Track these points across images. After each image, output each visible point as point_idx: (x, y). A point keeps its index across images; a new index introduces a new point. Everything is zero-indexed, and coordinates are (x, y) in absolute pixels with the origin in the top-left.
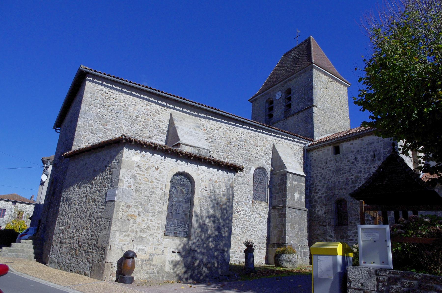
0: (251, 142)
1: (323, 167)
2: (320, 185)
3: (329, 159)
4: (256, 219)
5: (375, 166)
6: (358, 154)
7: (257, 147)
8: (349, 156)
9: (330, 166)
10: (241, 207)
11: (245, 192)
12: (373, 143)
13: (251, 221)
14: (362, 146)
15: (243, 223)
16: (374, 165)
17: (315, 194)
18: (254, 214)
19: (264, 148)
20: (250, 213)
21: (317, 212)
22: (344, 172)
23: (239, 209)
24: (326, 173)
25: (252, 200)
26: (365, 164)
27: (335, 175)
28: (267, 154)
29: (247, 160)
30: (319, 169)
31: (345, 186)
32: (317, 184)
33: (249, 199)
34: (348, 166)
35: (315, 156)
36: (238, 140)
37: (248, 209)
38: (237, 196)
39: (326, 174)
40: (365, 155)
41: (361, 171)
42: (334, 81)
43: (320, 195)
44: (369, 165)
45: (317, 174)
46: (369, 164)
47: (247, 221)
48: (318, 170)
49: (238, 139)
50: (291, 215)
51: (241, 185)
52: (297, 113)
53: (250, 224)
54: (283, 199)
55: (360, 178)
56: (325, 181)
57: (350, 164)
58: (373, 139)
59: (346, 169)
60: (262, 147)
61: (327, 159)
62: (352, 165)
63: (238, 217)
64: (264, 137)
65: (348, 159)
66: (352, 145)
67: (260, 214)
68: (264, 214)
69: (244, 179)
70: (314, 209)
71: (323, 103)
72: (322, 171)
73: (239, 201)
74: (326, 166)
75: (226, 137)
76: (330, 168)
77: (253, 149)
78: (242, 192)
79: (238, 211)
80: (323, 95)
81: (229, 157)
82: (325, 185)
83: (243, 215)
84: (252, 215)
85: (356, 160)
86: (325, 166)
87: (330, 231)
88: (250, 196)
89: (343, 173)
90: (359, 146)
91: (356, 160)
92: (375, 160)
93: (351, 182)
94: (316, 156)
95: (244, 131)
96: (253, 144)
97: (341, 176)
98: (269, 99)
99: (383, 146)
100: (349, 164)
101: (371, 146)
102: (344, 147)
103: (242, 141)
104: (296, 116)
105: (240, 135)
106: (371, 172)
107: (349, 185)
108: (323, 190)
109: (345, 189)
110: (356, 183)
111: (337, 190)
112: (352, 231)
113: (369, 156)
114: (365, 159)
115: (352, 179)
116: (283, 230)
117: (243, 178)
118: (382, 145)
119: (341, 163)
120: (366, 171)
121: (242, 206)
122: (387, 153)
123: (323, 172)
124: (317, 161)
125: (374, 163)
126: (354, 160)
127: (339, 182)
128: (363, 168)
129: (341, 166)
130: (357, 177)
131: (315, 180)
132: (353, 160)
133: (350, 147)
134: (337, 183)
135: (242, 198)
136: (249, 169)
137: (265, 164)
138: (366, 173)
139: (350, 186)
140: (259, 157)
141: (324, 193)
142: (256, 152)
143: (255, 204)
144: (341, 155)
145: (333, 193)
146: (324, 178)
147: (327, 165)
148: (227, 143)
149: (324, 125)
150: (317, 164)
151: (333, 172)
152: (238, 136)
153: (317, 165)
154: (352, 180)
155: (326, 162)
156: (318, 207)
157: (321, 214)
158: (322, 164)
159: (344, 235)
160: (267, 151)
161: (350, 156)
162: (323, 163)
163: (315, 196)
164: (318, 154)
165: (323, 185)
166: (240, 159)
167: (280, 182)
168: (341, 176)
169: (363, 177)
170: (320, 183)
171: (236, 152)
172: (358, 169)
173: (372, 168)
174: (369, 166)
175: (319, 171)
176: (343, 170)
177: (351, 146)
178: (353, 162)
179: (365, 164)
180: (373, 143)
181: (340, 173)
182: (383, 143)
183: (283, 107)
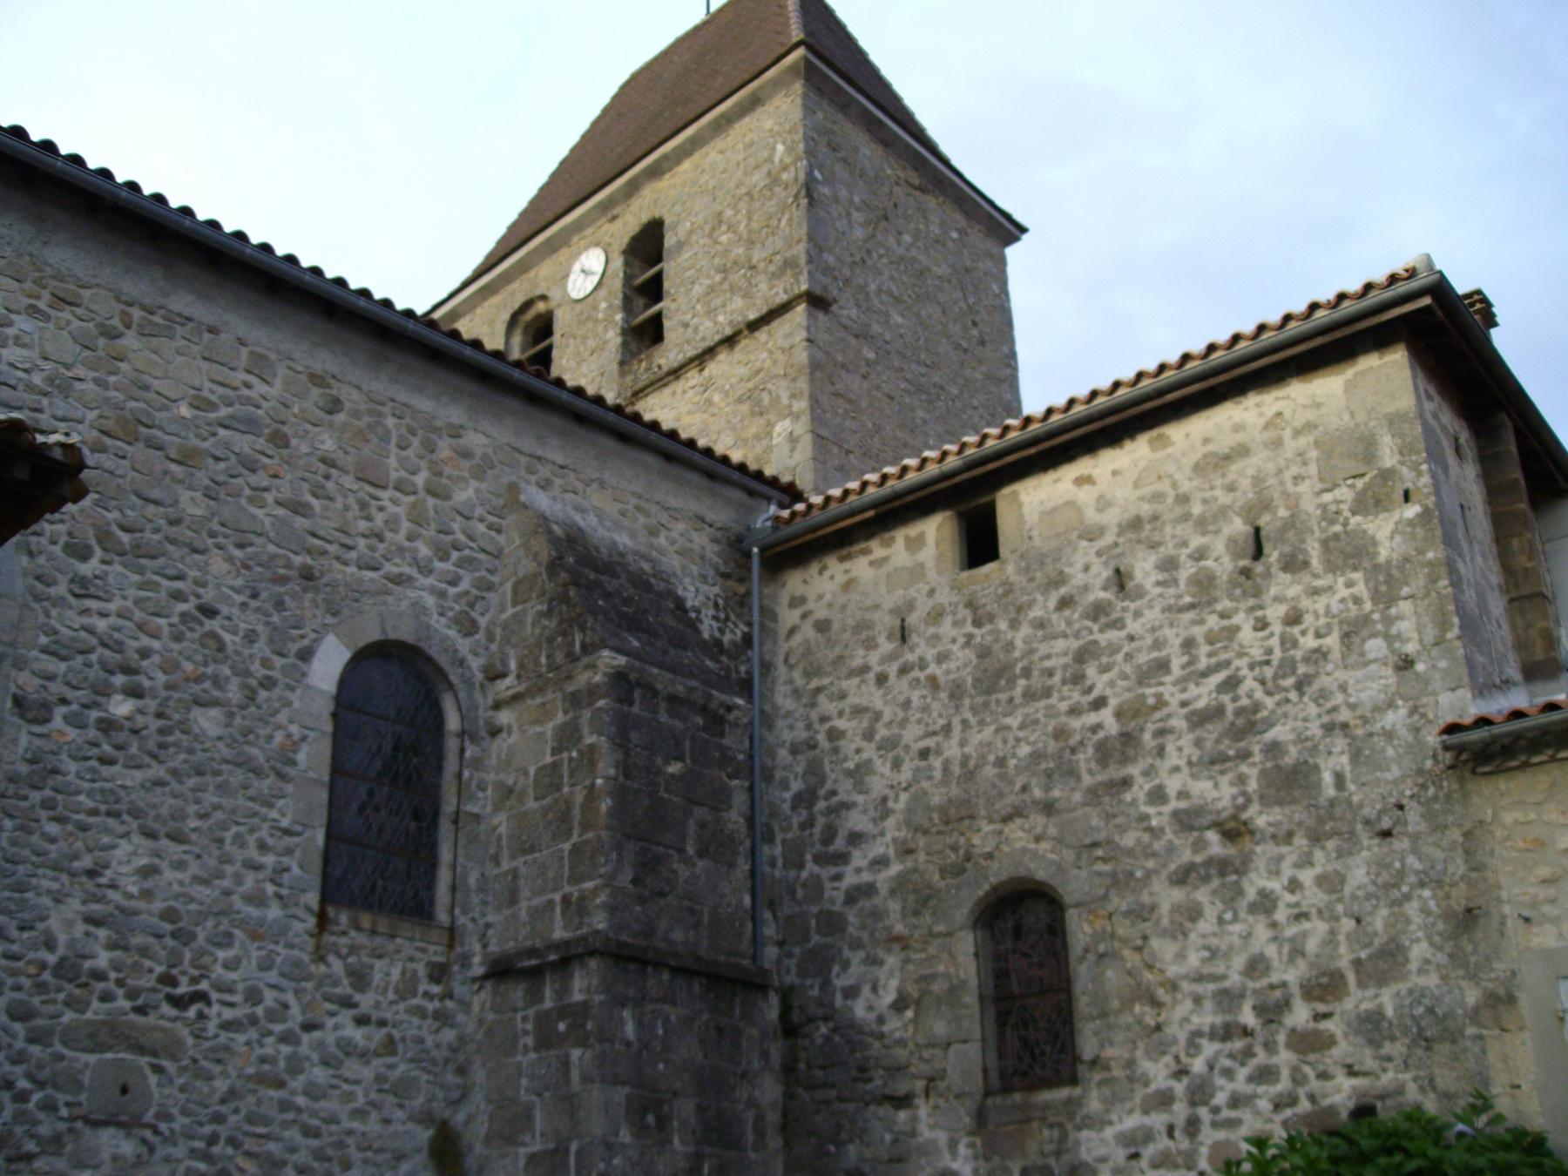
0: (328, 444)
1: (877, 669)
2: (860, 799)
3: (923, 607)
4: (352, 1068)
5: (1270, 619)
6: (1139, 542)
7: (379, 493)
8: (1067, 570)
9: (930, 654)
10: (206, 960)
11: (252, 831)
12: (1242, 451)
13: (297, 1083)
14: (1165, 486)
15: (223, 1101)
16: (1261, 607)
17: (826, 872)
18: (330, 1022)
19: (431, 502)
20: (295, 1010)
21: (839, 1000)
22: (1036, 681)
23: (194, 980)
24: (907, 704)
25: (312, 899)
26: (1192, 606)
27: (969, 716)
28: (455, 555)
29: (284, 580)
30: (855, 681)
31: (1048, 789)
32: (835, 800)
33: (285, 892)
34: (1065, 636)
35: (820, 597)
36: (212, 416)
37: (272, 976)
38: (180, 865)
39: (901, 714)
40: (1185, 544)
41: (1163, 666)
42: (930, 187)
43: (858, 871)
44: (1223, 615)
45: (840, 724)
46: (1219, 607)
47: (261, 1079)
48: (843, 696)
49: (212, 406)
50: (640, 1024)
51: (217, 773)
52: (705, 356)
53: (285, 1106)
54: (567, 889)
55: (1158, 715)
56: (897, 765)
57: (1077, 626)
58: (1238, 428)
59: (1048, 664)
60: (422, 494)
61: (910, 606)
62: (1091, 632)
63: (179, 1042)
64: (438, 423)
65: (1063, 591)
66: (1087, 487)
67: (382, 1023)
68: (416, 1021)
69: (247, 732)
70: (817, 982)
71: (867, 298)
72: (874, 697)
73: (193, 907)
74: (901, 661)
75: (112, 379)
76: (933, 669)
77: (340, 499)
78: (228, 835)
79: (183, 989)
80: (869, 251)
81: (125, 538)
82: (896, 800)
83: (227, 1026)
84: (309, 1027)
85: (1122, 587)
86: (891, 657)
87: (942, 1137)
88: (296, 870)
89: (1029, 696)
90: (1136, 485)
91: (1122, 587)
92: (1268, 575)
93: (1090, 750)
94: (828, 597)
95: (273, 356)
96: (349, 461)
97: (1014, 722)
98: (528, 304)
99: (1313, 469)
100: (1069, 623)
101: (1231, 477)
102: (1026, 509)
103: (250, 426)
104: (693, 378)
105: (238, 383)
106: (1237, 663)
107: (1078, 778)
108: (882, 834)
109: (1048, 808)
110: (1125, 760)
111: (987, 828)
112: (1111, 1123)
113: (1219, 547)
114: (1187, 571)
115: (1095, 728)
116: (567, 1151)
117: (238, 721)
118: (1305, 464)
119: (1014, 624)
120: (1203, 663)
121: (222, 954)
122: (1347, 513)
123: (878, 704)
124: (836, 626)
125: (1256, 595)
126: (1105, 589)
127: (1001, 762)
128: (1178, 641)
129: (1010, 646)
130: (1131, 713)
131: (827, 768)
132: (1102, 595)
133: (1071, 504)
134: (990, 771)
135: (226, 883)
136: (294, 647)
137: (439, 624)
138: (1205, 674)
139: (1087, 780)
140: (390, 568)
141: (891, 852)
142: (363, 525)
143: (343, 941)
144: (1010, 569)
145: (955, 848)
146: (888, 745)
147: (912, 649)
148: (117, 430)
149: (878, 429)
150: (837, 651)
151: (956, 693)
152: (220, 390)
153: (840, 659)
154: (1101, 735)
155: (903, 628)
156: (846, 965)
157: (872, 1017)
158: (870, 644)
159: (1052, 1161)
160: (456, 526)
161: (1079, 566)
162: (882, 640)
163: (828, 885)
164: (841, 579)
165: (885, 800)
166: (218, 565)
167: (549, 759)
168: (1014, 722)
169: (1184, 704)
170: (860, 787)
171: (192, 505)
172: (1139, 650)
173: (1247, 634)
174: (1225, 623)
175: (853, 700)
176: (1027, 672)
177: (1085, 495)
178: (1098, 611)
179: (1192, 606)
180: (1242, 451)
181: (1003, 697)
182: (1316, 442)
183: (614, 338)
